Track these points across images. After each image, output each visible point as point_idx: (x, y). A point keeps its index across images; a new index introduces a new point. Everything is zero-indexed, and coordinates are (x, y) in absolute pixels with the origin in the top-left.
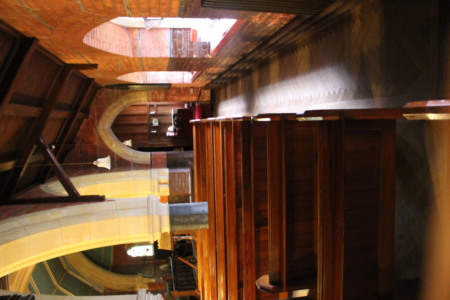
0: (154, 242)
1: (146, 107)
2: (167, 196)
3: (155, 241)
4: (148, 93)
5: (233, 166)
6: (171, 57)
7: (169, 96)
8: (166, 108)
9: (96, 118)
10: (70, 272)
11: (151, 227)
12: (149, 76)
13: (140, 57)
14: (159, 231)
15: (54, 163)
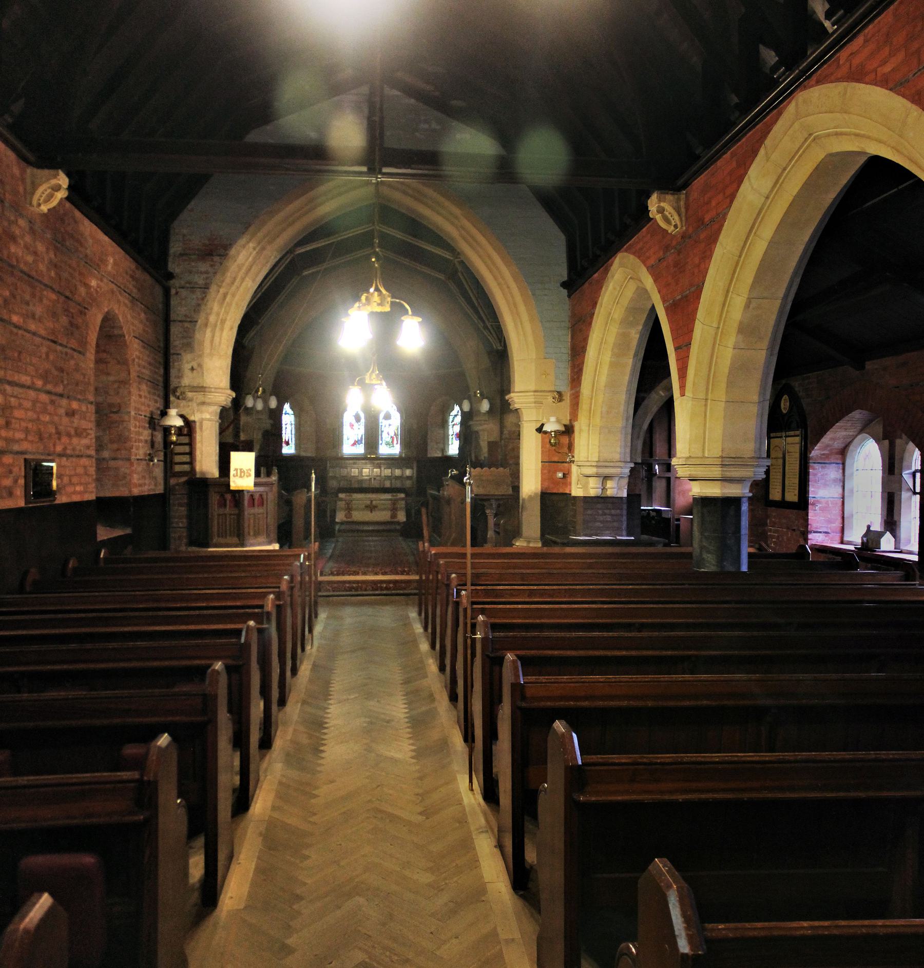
1: (666, 458)
5: (449, 631)
8: (664, 494)
10: (442, 277)
11: (736, 461)
12: (823, 468)
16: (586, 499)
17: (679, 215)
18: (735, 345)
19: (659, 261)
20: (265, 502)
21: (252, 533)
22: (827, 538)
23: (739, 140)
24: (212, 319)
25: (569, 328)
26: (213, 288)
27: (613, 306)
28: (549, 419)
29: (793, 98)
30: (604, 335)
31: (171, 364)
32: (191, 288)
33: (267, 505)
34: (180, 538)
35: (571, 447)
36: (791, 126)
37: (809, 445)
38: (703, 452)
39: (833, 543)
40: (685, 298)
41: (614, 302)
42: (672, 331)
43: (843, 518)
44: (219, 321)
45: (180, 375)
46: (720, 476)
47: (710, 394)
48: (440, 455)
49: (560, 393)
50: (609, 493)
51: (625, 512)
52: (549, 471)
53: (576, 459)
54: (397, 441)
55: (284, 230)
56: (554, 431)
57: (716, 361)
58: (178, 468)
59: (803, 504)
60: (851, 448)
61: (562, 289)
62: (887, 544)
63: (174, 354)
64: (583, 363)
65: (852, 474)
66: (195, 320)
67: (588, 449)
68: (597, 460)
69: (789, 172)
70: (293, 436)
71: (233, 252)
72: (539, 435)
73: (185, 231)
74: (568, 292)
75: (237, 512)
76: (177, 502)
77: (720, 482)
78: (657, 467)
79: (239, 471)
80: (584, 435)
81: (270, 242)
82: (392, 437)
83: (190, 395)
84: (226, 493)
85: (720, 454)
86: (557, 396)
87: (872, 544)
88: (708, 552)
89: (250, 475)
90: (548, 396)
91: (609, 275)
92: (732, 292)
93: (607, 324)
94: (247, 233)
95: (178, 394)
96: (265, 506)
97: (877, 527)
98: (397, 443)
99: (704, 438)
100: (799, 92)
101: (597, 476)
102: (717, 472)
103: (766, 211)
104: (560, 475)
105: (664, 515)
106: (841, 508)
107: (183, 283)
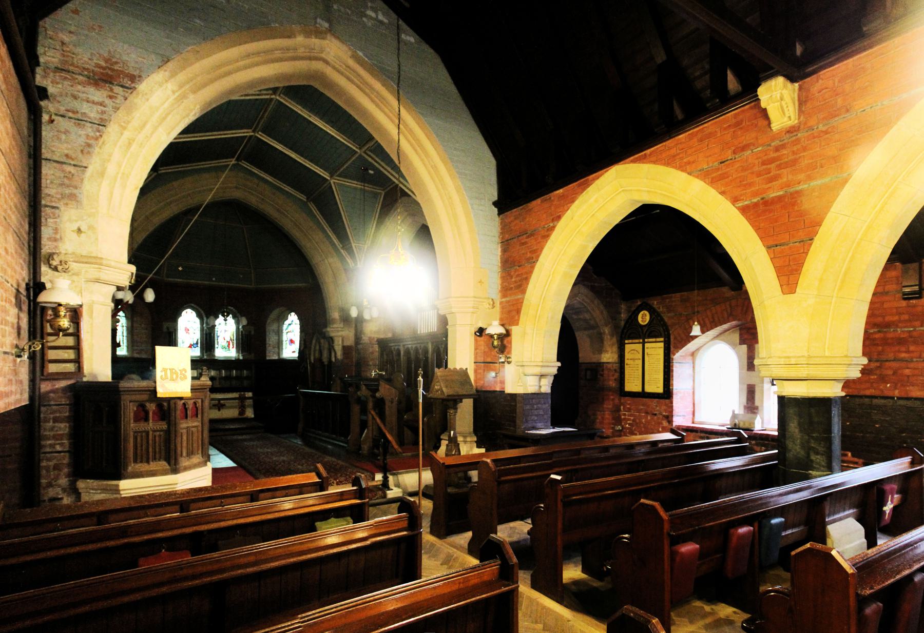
4: (616, 363)
7: (612, 395)
9: (593, 284)
15: (247, 136)
20: (200, 412)
21: (184, 454)
24: (111, 169)
26: (112, 130)
31: (43, 220)
32: (75, 119)
33: (202, 413)
34: (56, 467)
37: (672, 349)
43: (694, 404)
44: (120, 175)
45: (58, 237)
48: (276, 358)
54: (233, 345)
55: (212, 81)
58: (52, 368)
59: (667, 394)
61: (493, 207)
63: (46, 206)
64: (531, 272)
66: (86, 165)
70: (125, 338)
71: (142, 87)
73: (66, 38)
74: (499, 211)
75: (165, 427)
76: (52, 416)
79: (169, 372)
81: (194, 92)
82: (229, 343)
83: (74, 266)
84: (150, 401)
88: (817, 453)
89: (186, 378)
94: (165, 68)
95: (54, 263)
96: (199, 416)
98: (233, 348)
107: (62, 109)
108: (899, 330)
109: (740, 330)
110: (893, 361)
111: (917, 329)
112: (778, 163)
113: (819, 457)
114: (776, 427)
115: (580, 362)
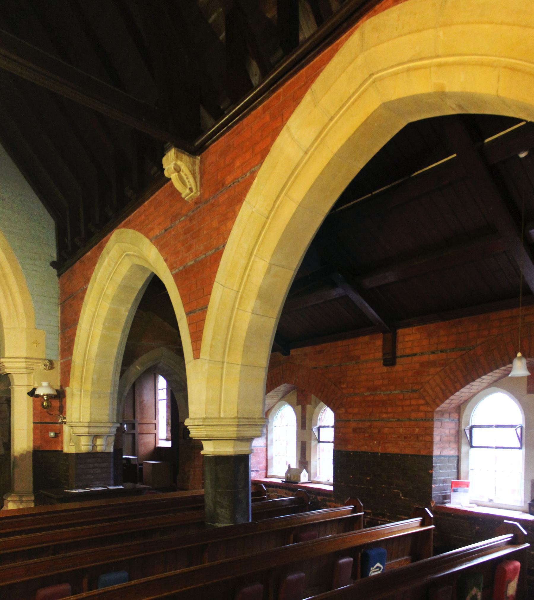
0: (187, 426)
1: (132, 419)
2: (431, 455)
3: (188, 428)
6: (434, 457)
11: (249, 422)
13: (434, 420)
14: (239, 435)
16: (79, 456)
17: (195, 177)
18: (253, 310)
19: (166, 231)
22: (257, 475)
23: (274, 91)
25: (58, 304)
27: (107, 282)
28: (41, 384)
29: (356, 28)
30: (96, 309)
35: (62, 410)
36: (352, 61)
38: (219, 413)
39: (261, 478)
40: (201, 263)
41: (108, 279)
42: (182, 296)
43: (267, 460)
46: (235, 436)
47: (226, 357)
49: (51, 362)
50: (99, 449)
51: (112, 465)
52: (41, 431)
53: (67, 420)
56: (47, 395)
57: (234, 324)
60: (273, 411)
61: (51, 268)
62: (304, 477)
65: (272, 429)
67: (80, 411)
68: (89, 421)
69: (336, 122)
72: (31, 399)
74: (58, 272)
77: (233, 441)
78: (125, 426)
80: (76, 399)
85: (235, 415)
86: (48, 364)
87: (294, 478)
88: (222, 507)
90: (39, 363)
91: (104, 251)
92: (255, 256)
93: (99, 299)
97: (294, 466)
99: (220, 400)
100: (366, 20)
101: (89, 435)
102: (232, 432)
103: (303, 168)
104: (52, 434)
105: (133, 462)
106: (265, 453)
108: (382, 393)
109: (298, 391)
110: (378, 420)
111: (393, 392)
112: (192, 232)
113: (223, 510)
114: (332, 481)
115: (180, 422)
